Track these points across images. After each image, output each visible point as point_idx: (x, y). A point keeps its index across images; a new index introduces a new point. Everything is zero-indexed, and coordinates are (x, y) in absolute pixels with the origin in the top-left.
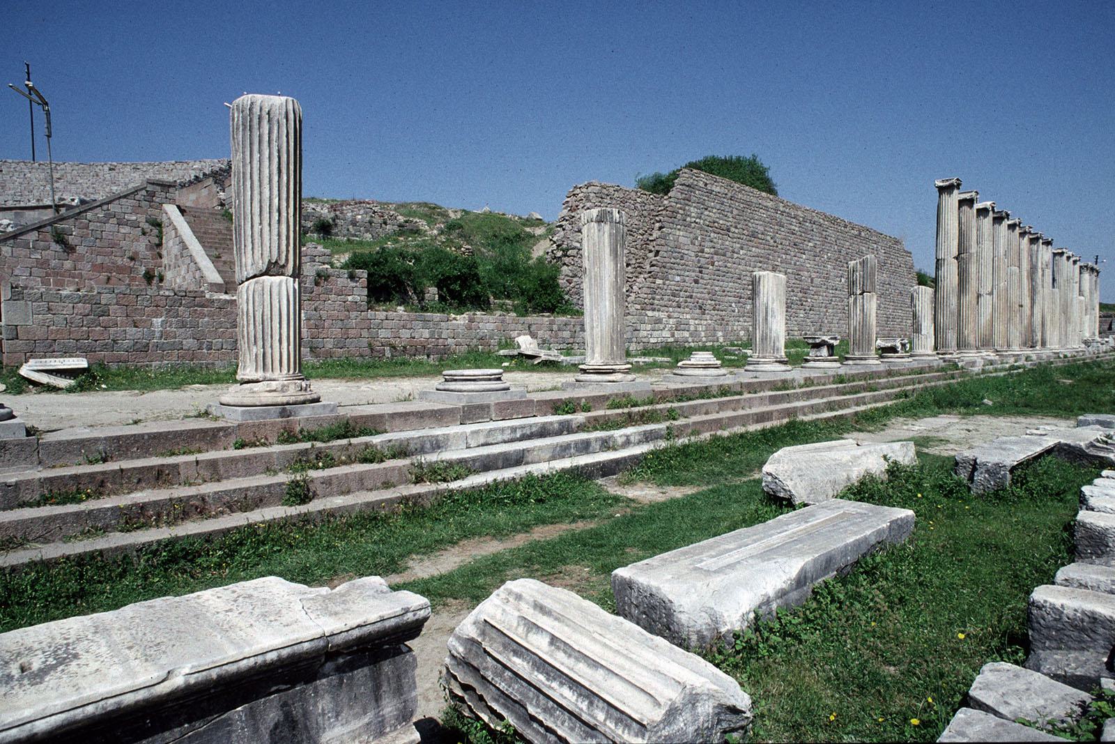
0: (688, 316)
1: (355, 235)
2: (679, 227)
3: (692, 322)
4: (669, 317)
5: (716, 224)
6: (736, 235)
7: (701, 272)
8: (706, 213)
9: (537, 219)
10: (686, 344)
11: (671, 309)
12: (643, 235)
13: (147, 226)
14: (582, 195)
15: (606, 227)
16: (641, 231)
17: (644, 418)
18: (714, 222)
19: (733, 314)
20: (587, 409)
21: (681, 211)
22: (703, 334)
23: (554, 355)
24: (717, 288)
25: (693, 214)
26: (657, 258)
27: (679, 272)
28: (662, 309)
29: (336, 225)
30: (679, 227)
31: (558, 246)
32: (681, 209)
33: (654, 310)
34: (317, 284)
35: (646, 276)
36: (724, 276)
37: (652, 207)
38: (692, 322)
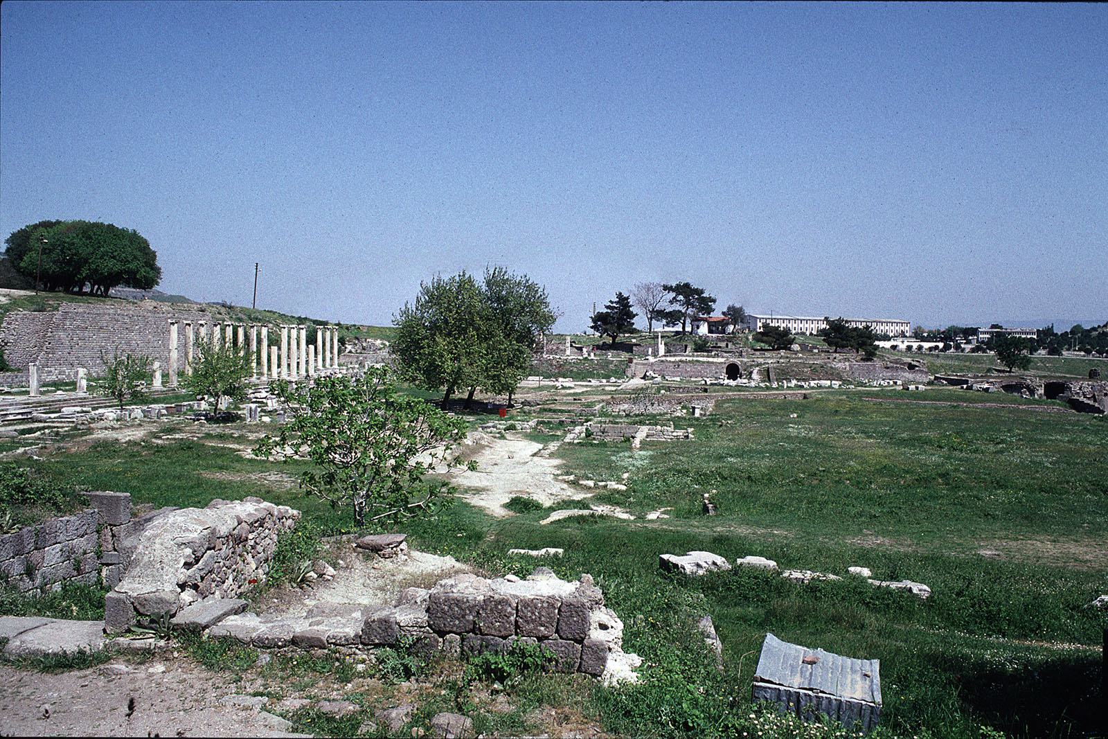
17: (44, 406)
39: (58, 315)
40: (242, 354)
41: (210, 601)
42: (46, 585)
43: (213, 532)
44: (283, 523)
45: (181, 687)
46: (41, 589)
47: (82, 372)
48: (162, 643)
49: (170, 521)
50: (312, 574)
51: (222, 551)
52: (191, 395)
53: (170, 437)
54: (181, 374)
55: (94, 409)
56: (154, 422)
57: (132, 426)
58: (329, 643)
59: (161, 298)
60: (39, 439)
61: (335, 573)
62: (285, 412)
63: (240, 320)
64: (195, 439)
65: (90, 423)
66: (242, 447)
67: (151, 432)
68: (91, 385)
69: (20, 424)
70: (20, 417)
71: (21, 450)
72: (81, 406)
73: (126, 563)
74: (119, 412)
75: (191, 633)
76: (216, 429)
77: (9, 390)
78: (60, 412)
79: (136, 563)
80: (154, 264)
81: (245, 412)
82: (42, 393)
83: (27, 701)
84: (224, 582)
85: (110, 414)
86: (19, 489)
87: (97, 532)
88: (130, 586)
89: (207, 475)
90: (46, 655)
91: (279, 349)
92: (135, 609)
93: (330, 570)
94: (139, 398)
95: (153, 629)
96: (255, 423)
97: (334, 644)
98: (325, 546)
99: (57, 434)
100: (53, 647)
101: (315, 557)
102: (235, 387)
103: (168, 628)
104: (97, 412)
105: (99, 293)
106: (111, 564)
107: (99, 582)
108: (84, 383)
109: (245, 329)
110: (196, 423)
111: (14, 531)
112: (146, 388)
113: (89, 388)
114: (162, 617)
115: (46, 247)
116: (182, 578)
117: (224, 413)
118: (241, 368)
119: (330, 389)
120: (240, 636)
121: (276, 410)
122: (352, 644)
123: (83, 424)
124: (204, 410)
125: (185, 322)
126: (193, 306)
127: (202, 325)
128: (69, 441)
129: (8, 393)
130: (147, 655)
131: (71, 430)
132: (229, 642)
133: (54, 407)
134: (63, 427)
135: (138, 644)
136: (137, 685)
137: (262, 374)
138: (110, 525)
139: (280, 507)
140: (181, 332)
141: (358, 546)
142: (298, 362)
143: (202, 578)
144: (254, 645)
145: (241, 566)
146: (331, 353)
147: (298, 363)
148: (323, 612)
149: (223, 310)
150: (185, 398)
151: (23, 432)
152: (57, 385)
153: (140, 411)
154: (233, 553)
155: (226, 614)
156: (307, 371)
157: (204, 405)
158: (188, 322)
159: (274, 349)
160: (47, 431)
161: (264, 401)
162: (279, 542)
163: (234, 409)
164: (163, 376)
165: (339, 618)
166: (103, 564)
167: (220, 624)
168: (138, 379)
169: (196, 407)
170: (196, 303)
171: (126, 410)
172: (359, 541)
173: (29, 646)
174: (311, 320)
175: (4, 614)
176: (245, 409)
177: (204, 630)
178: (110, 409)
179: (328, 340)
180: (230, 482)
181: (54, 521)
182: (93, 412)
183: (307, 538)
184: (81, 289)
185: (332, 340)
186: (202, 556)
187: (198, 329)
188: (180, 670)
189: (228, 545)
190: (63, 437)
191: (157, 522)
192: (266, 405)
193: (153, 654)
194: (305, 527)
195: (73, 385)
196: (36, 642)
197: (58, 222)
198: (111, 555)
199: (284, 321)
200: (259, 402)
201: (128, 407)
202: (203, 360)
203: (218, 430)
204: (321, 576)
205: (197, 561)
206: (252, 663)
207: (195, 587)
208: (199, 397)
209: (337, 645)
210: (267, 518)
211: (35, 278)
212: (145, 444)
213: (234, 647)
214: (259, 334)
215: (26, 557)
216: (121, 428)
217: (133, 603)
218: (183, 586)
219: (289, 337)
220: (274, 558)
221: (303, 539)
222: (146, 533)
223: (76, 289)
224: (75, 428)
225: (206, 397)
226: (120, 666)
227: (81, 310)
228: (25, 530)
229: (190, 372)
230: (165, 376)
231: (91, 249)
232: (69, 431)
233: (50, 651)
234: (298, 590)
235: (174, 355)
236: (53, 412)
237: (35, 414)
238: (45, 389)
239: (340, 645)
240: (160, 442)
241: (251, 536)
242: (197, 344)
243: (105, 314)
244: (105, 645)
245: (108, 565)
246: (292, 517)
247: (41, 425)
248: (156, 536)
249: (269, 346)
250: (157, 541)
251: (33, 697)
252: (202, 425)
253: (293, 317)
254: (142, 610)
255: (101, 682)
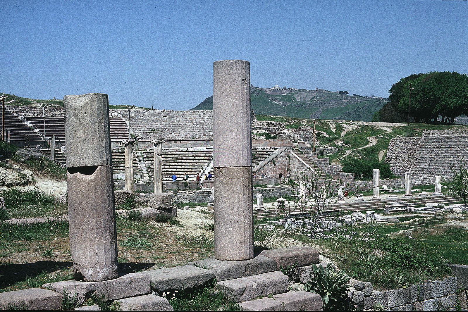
0: (427, 176)
1: (328, 154)
2: (423, 150)
3: (428, 178)
4: (421, 177)
5: (436, 146)
6: (443, 148)
7: (431, 162)
8: (433, 143)
9: (366, 125)
10: (426, 184)
11: (421, 175)
12: (412, 151)
13: (287, 158)
14: (395, 142)
15: (409, 175)
16: (412, 150)
17: (414, 202)
18: (435, 146)
19: (442, 174)
20: (407, 201)
21: (424, 145)
22: (432, 181)
23: (391, 190)
24: (436, 166)
25: (428, 145)
26: (417, 160)
27: (424, 163)
28: (419, 175)
29: (324, 151)
30: (423, 150)
31: (388, 158)
32: (424, 144)
33: (416, 175)
34: (347, 177)
35: (414, 165)
36: (439, 162)
37: (415, 142)
38: (428, 178)
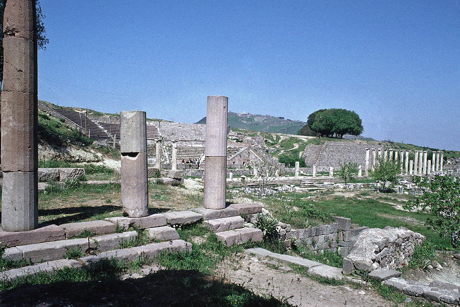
39: (324, 146)
40: (396, 163)
41: (384, 269)
42: (319, 250)
43: (388, 240)
44: (417, 240)
45: (372, 303)
46: (317, 251)
47: (332, 168)
48: (364, 282)
49: (370, 233)
50: (430, 266)
51: (390, 249)
52: (374, 180)
53: (364, 197)
54: (369, 171)
55: (335, 183)
56: (358, 190)
57: (350, 191)
58: (441, 301)
59: (362, 139)
60: (316, 194)
61: (442, 268)
62: (415, 190)
63: (396, 148)
64: (375, 199)
65: (334, 189)
66: (395, 204)
67: (357, 195)
68: (335, 174)
69: (309, 187)
70: (309, 185)
71: (309, 197)
72: (331, 182)
73: (352, 247)
74: (344, 185)
75: (376, 281)
76: (384, 195)
77: (306, 174)
78: (323, 184)
79: (355, 248)
80: (361, 125)
81: (397, 189)
82: (317, 176)
83: (315, 293)
84: (390, 262)
85: (341, 186)
86: (311, 213)
87: (337, 232)
88: (353, 256)
89: (379, 215)
90: (321, 277)
91: (414, 161)
92: (354, 266)
93: (440, 266)
94: (352, 180)
95: (361, 276)
96: (401, 194)
97: (444, 301)
98: (437, 254)
99: (322, 192)
100: (324, 275)
101: (432, 258)
102: (393, 178)
103: (367, 277)
104: (336, 185)
105: (339, 137)
106: (342, 246)
107: (337, 252)
108: (332, 173)
109: (398, 152)
110: (375, 192)
111: (309, 228)
112: (356, 176)
113: (334, 175)
114: (365, 272)
115: (321, 119)
116: (374, 257)
117: (387, 189)
118: (396, 169)
119: (441, 182)
120: (398, 287)
121: (411, 189)
122: (454, 304)
123: (331, 189)
124: (379, 187)
125: (372, 149)
126: (376, 142)
127: (379, 150)
128: (326, 196)
129: (306, 175)
130: (358, 286)
131: (327, 191)
132: (393, 289)
133: (320, 182)
134: (324, 190)
135: (355, 281)
136: (354, 297)
137: (405, 172)
138: (342, 230)
139: (416, 233)
140: (371, 153)
141: (455, 257)
142: (425, 168)
143: (382, 259)
144: (404, 293)
145: (398, 256)
146: (439, 164)
147: (422, 168)
148: (438, 285)
149: (389, 144)
150: (371, 181)
151: (310, 190)
152: (322, 173)
153: (352, 185)
154: (395, 250)
155: (392, 276)
156: (427, 172)
157: (379, 185)
158: (374, 149)
159: (412, 161)
160: (318, 191)
161: (406, 184)
162: (415, 249)
163: (392, 187)
164: (362, 172)
165: (446, 290)
166: (339, 246)
167: (389, 280)
168: (353, 172)
169: (375, 185)
170: (377, 141)
171: (347, 185)
172: (455, 255)
173: (315, 272)
174: (430, 149)
175: (305, 258)
176: (397, 188)
177: (382, 281)
178: (341, 184)
179: (438, 158)
180: (389, 219)
181: (323, 226)
182: (335, 185)
183: (429, 249)
184: (332, 136)
185: (440, 158)
186: (382, 250)
187: (378, 152)
188: (371, 295)
189: (393, 246)
190: (324, 194)
191: (365, 232)
192: (407, 186)
193: (361, 286)
194: (427, 244)
195: (328, 174)
196: (318, 271)
197: (325, 110)
198: (341, 243)
199: (416, 149)
200: (403, 185)
201: (348, 184)
202: (379, 166)
203: (385, 196)
204: (435, 268)
205: (380, 251)
206: (403, 301)
207: (379, 262)
208: (377, 181)
209: (445, 302)
210: (410, 237)
211: (316, 132)
212: (354, 199)
213: (395, 291)
214: (405, 155)
215: (312, 238)
216: (345, 192)
217: (353, 264)
218: (374, 261)
219: (419, 156)
220: (413, 256)
221: (427, 250)
222: (360, 236)
223: (331, 136)
224: (328, 191)
225: (380, 181)
226: (348, 288)
227: (332, 144)
228: (313, 228)
229: (374, 170)
230: (363, 171)
231: (336, 120)
232: (326, 191)
233: (323, 276)
234: (423, 272)
235: (367, 163)
236: (320, 184)
237: (314, 184)
238: (318, 174)
239: (447, 303)
240: (360, 199)
241: (403, 244)
242: (377, 158)
243: (341, 146)
244: (342, 279)
245: (341, 246)
246: (422, 239)
247: (316, 188)
248: (364, 238)
249: (409, 160)
250: (364, 240)
251: (316, 292)
252: (378, 193)
253: (421, 147)
254: (357, 267)
255: (340, 292)
